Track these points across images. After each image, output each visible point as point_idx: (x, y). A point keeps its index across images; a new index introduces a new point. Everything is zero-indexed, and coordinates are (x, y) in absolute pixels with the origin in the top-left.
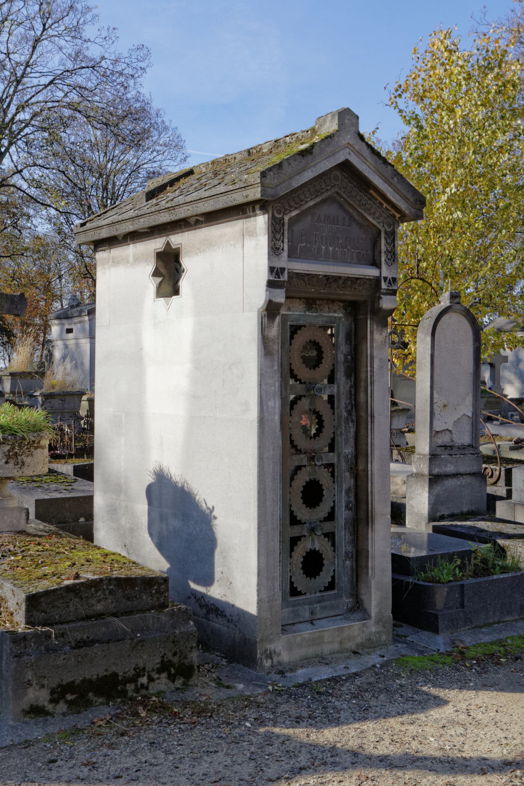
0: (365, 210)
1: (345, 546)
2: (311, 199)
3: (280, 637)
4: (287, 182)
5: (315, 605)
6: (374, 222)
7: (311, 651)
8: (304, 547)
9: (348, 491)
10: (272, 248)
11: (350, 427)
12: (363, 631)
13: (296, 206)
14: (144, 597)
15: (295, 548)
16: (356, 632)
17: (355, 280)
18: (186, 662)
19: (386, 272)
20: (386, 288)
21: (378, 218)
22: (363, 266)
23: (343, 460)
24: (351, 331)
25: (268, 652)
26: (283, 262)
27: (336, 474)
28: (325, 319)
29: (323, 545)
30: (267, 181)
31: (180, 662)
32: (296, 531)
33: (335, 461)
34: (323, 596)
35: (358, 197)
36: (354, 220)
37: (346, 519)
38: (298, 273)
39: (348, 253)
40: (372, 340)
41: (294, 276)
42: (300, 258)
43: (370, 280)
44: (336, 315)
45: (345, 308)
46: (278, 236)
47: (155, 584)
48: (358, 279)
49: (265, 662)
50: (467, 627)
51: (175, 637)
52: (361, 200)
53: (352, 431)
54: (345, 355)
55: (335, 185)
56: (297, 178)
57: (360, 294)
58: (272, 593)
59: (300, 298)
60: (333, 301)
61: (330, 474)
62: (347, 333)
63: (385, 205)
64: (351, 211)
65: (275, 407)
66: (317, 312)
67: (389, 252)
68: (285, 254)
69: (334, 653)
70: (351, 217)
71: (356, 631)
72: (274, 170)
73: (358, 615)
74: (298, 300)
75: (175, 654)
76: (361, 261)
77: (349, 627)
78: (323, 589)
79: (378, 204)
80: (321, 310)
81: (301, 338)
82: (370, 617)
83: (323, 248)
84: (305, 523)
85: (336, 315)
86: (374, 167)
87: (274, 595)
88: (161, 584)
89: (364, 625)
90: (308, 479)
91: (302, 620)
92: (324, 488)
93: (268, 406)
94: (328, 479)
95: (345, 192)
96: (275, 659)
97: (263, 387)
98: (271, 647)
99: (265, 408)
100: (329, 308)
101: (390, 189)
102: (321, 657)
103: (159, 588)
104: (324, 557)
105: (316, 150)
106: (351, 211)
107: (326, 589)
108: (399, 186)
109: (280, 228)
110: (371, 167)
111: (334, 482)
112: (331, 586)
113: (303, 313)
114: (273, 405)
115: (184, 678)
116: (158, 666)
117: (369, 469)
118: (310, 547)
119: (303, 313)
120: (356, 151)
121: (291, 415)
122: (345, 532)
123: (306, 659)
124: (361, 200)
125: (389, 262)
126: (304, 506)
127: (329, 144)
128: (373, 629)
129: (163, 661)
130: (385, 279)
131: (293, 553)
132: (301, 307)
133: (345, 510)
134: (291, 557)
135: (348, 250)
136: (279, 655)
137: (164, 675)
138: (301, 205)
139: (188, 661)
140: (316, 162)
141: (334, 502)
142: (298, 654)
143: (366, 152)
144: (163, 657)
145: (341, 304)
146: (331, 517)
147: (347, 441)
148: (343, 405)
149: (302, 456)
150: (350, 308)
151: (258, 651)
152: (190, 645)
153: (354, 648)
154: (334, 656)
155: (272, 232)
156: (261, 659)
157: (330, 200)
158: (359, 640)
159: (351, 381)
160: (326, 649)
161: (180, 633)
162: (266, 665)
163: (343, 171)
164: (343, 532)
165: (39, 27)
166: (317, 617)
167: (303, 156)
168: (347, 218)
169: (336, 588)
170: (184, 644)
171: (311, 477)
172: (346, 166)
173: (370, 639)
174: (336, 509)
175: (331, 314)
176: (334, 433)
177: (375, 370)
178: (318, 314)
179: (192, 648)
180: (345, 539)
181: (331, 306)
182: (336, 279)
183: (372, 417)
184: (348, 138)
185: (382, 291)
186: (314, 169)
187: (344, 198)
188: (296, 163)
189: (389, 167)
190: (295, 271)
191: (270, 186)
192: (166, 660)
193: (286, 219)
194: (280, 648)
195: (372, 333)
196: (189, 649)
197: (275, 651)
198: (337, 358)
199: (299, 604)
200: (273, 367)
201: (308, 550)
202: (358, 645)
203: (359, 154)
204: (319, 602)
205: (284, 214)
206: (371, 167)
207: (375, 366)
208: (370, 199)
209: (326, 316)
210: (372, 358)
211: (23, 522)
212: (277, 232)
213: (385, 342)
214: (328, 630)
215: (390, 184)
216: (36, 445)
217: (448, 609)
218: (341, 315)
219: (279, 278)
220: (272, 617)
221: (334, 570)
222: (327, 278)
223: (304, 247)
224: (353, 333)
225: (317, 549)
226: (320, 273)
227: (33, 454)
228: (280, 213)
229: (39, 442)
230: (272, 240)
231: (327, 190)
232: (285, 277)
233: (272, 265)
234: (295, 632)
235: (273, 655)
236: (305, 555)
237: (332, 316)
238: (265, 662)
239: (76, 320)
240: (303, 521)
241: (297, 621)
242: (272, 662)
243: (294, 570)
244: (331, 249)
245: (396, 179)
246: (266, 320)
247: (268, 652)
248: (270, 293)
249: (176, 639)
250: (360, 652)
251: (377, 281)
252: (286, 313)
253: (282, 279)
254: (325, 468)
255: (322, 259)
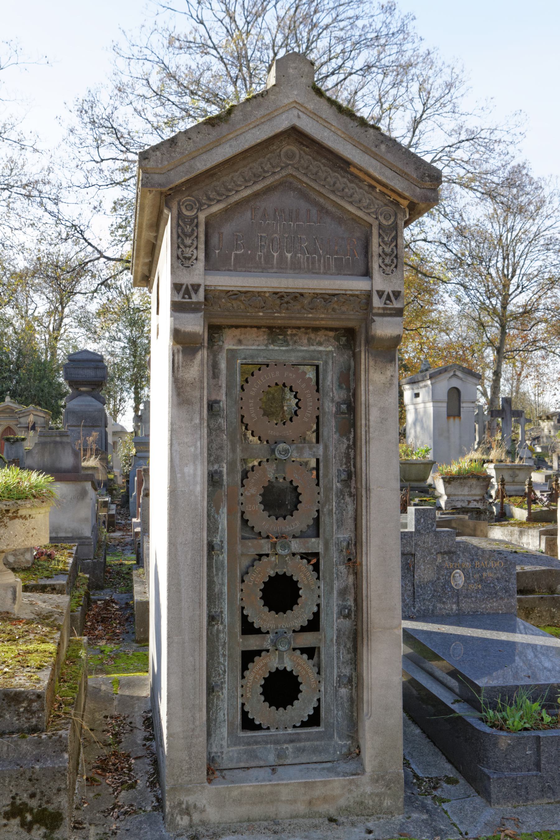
0: (342, 197)
1: (339, 668)
2: (246, 187)
3: (203, 787)
4: (187, 164)
5: (285, 746)
6: (359, 213)
7: (257, 811)
8: (266, 665)
9: (343, 593)
10: (178, 258)
11: (346, 504)
12: (350, 791)
13: (218, 198)
14: (7, 716)
15: (250, 665)
16: (338, 792)
17: (327, 298)
18: (51, 808)
19: (379, 282)
20: (382, 305)
21: (367, 207)
22: (356, 277)
23: (333, 549)
24: (349, 369)
25: (184, 806)
26: (197, 275)
27: (322, 567)
28: (300, 354)
29: (298, 663)
30: (151, 164)
31: (40, 806)
32: (253, 643)
33: (321, 549)
34: (298, 734)
35: (329, 179)
36: (327, 212)
37: (339, 630)
38: (229, 291)
39: (319, 261)
40: (367, 380)
41: (223, 295)
42: (235, 270)
43: (357, 296)
44: (321, 348)
45: (337, 339)
46: (188, 241)
47: (23, 701)
48: (334, 295)
49: (178, 818)
50: (546, 800)
51: (33, 773)
52: (334, 184)
53: (351, 508)
54: (338, 403)
55: (287, 165)
56: (204, 157)
57: (350, 317)
58: (191, 726)
59: (258, 327)
60: (316, 329)
61: (311, 568)
62: (342, 372)
63: (379, 188)
64: (322, 200)
65: (195, 475)
66: (288, 345)
67: (386, 255)
68: (200, 265)
69: (296, 817)
70: (322, 210)
71: (336, 789)
72: (164, 149)
73: (350, 766)
74: (256, 329)
75: (33, 796)
76: (342, 269)
77: (325, 783)
78: (298, 724)
79: (367, 188)
80: (295, 342)
81: (262, 381)
82: (364, 771)
83: (275, 255)
84: (268, 633)
85: (321, 348)
86: (344, 133)
87: (193, 730)
88: (32, 701)
89: (351, 782)
90: (272, 573)
91: (262, 763)
92: (299, 586)
93: (183, 474)
94: (308, 574)
95: (305, 174)
96: (196, 817)
97: (176, 447)
98: (189, 799)
99: (179, 475)
100: (309, 340)
101: (374, 162)
102: (273, 820)
103: (29, 705)
104: (300, 680)
105: (236, 116)
106: (322, 200)
107: (304, 725)
108: (389, 157)
109: (193, 230)
110: (339, 133)
111: (318, 578)
112: (314, 720)
113: (265, 348)
114: (192, 471)
115: (47, 828)
116: (8, 808)
117: (364, 563)
118: (276, 665)
119: (265, 348)
120: (310, 112)
121: (243, 486)
122: (338, 648)
123: (249, 820)
124: (334, 184)
125: (388, 269)
126: (266, 609)
127: (259, 106)
128: (368, 789)
129: (13, 804)
130: (380, 294)
131: (247, 673)
132: (265, 337)
133: (338, 618)
134: (243, 677)
135: (320, 256)
136: (203, 811)
137: (17, 821)
138: (228, 196)
139: (53, 806)
140: (238, 132)
141: (318, 605)
142: (233, 813)
143: (327, 112)
144: (13, 798)
145: (332, 334)
146: (313, 625)
147: (341, 523)
148: (333, 470)
149: (263, 541)
150: (344, 339)
151: (168, 803)
152: (57, 786)
153: (332, 812)
154: (296, 821)
155: (179, 236)
156: (172, 815)
157: (283, 185)
158: (342, 802)
159: (348, 440)
160: (284, 810)
161: (41, 768)
162: (180, 822)
163: (302, 144)
164: (335, 648)
165: (420, 108)
166: (288, 761)
167: (213, 126)
168: (314, 211)
169: (322, 724)
170: (47, 783)
171: (277, 570)
172: (295, 134)
173: (362, 803)
174: (322, 616)
175: (312, 348)
176: (318, 511)
177: (372, 423)
178: (290, 347)
179: (59, 790)
180: (338, 658)
181: (312, 336)
182: (298, 296)
183: (368, 490)
184: (297, 94)
185: (375, 311)
186: (234, 143)
187: (306, 183)
188: (200, 136)
189: (371, 131)
190: (220, 288)
191: (158, 171)
192: (18, 802)
193: (202, 217)
194: (205, 802)
195: (367, 371)
196: (55, 791)
197: (195, 806)
198: (323, 409)
199: (257, 743)
200: (192, 420)
201: (274, 670)
202: (340, 810)
203: (314, 115)
204: (292, 741)
205: (199, 209)
206: (339, 133)
207: (372, 418)
208: (351, 181)
209: (303, 351)
210: (367, 407)
211: (9, 601)
212: (186, 235)
213: (391, 384)
214: (287, 785)
215: (375, 156)
216: (10, 514)
217: (514, 770)
218: (330, 348)
219: (190, 298)
220: (190, 758)
221: (319, 700)
222: (279, 295)
223: (242, 255)
224: (351, 373)
225: (289, 669)
226: (265, 290)
227: (8, 525)
228: (192, 209)
229: (16, 511)
230: (179, 247)
231: (274, 173)
232: (200, 296)
233: (177, 281)
234: (233, 782)
235: (192, 811)
236: (267, 675)
237: (314, 351)
238: (178, 818)
239: (421, 384)
240: (263, 630)
241: (253, 764)
242: (191, 820)
243: (248, 695)
244: (289, 255)
245: (383, 147)
246: (180, 357)
247: (184, 806)
248: (175, 319)
249: (34, 776)
250: (342, 819)
251: (369, 295)
252: (235, 347)
253: (194, 299)
254: (302, 558)
255: (274, 270)
